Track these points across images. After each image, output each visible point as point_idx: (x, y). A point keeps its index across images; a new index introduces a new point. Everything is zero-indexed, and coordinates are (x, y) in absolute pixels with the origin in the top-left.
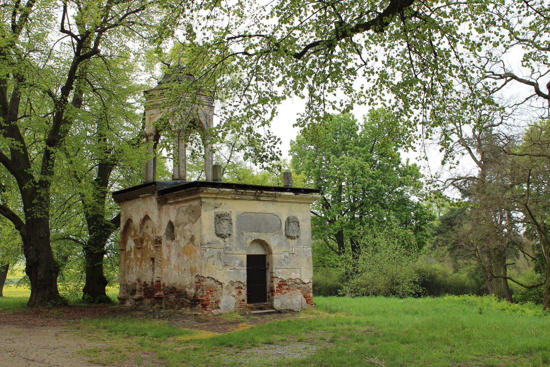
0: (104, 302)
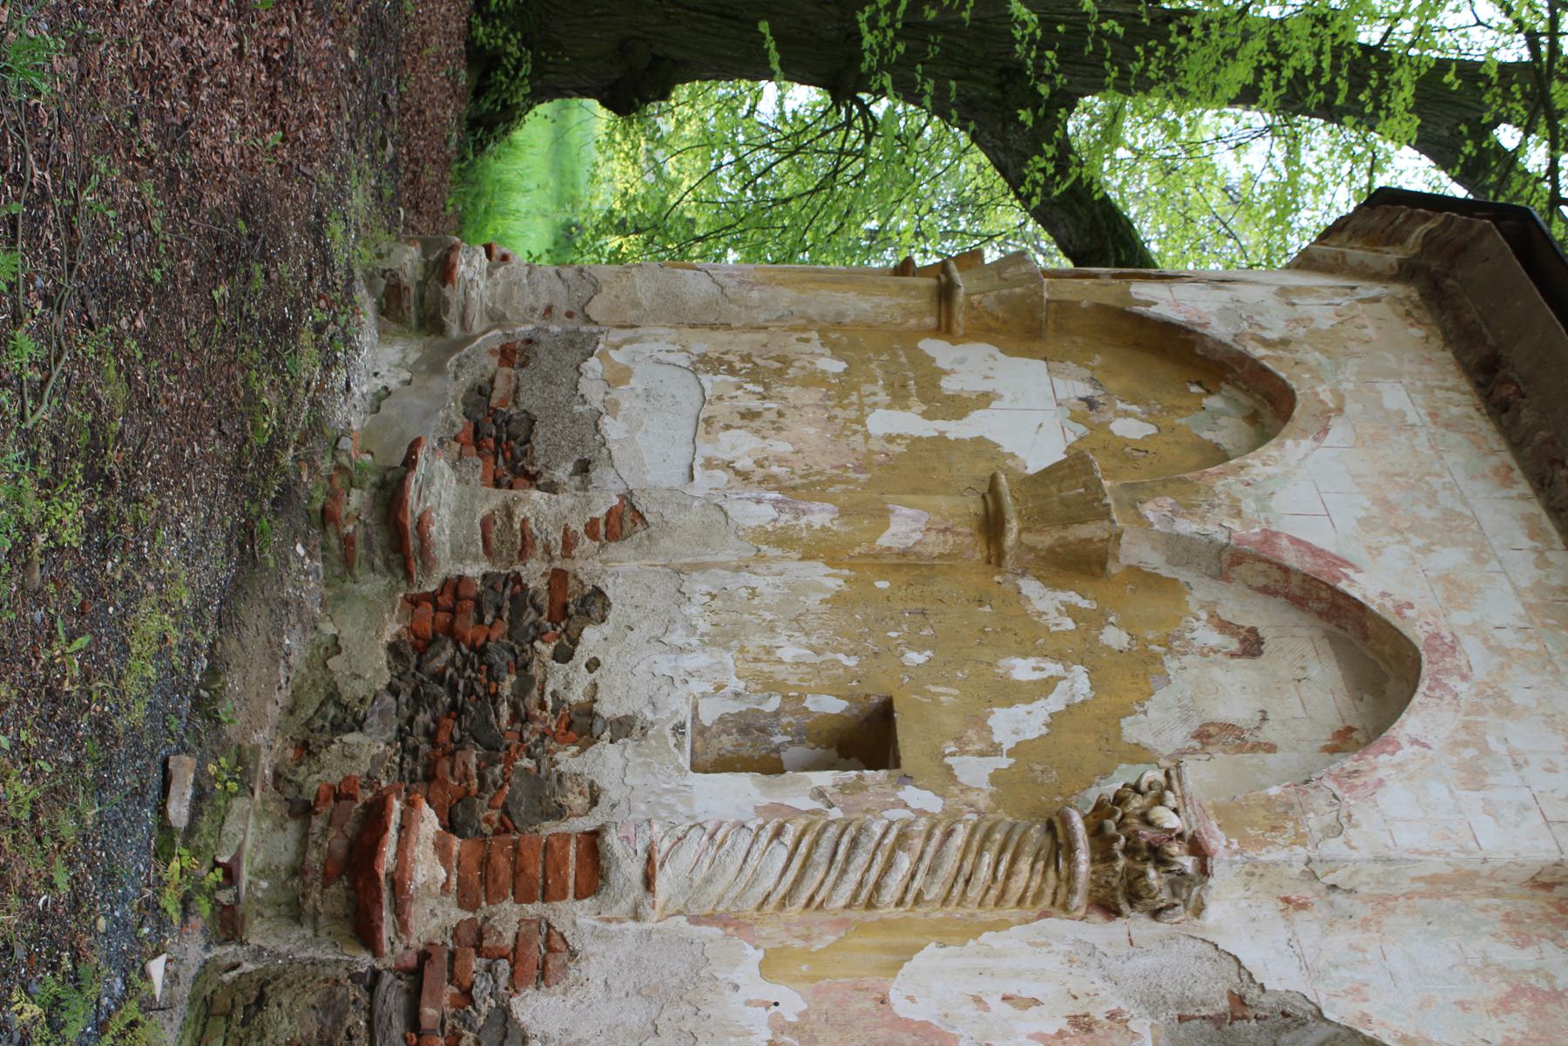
0: (478, 92)
